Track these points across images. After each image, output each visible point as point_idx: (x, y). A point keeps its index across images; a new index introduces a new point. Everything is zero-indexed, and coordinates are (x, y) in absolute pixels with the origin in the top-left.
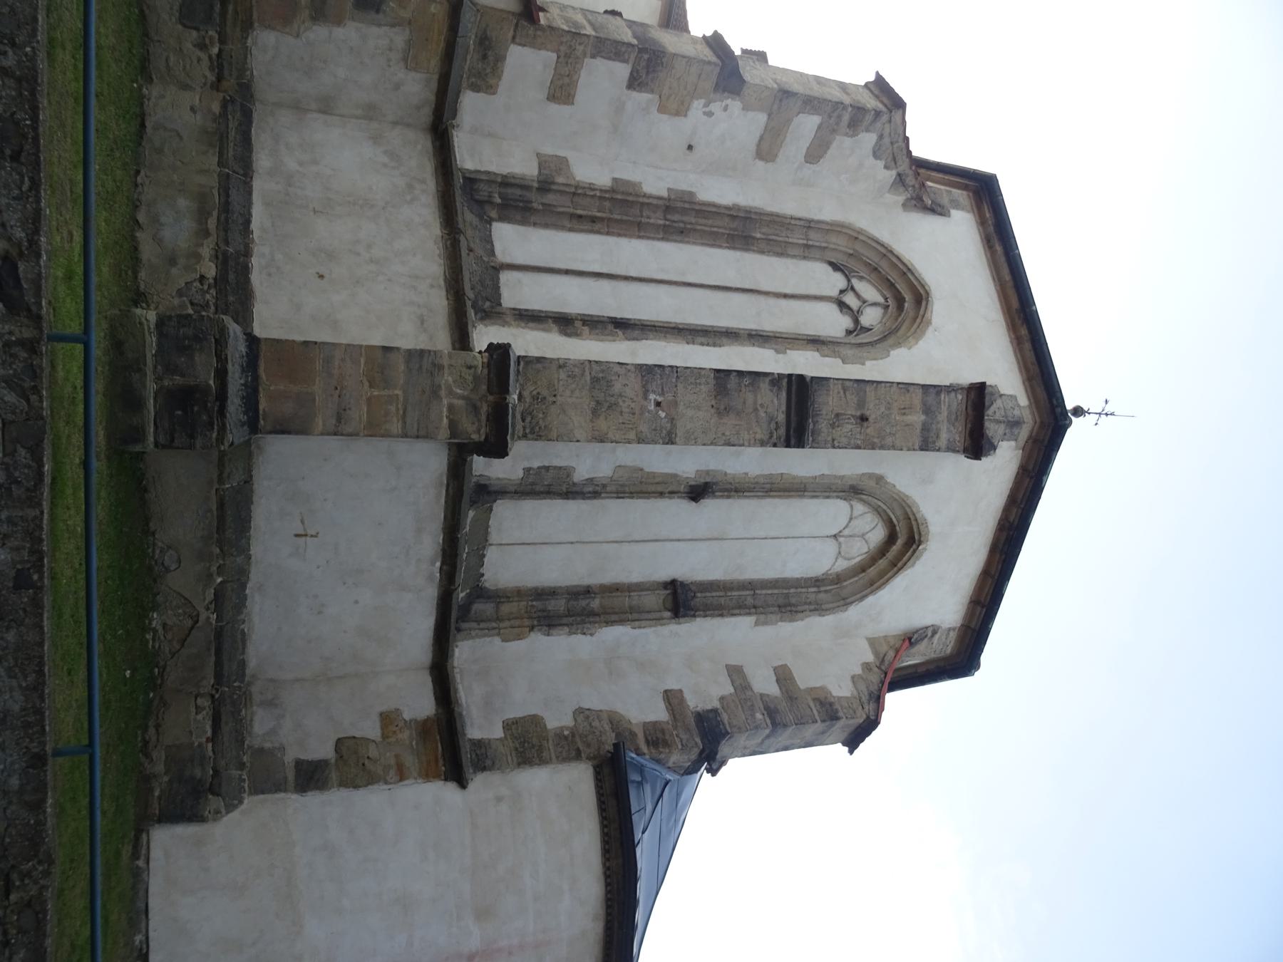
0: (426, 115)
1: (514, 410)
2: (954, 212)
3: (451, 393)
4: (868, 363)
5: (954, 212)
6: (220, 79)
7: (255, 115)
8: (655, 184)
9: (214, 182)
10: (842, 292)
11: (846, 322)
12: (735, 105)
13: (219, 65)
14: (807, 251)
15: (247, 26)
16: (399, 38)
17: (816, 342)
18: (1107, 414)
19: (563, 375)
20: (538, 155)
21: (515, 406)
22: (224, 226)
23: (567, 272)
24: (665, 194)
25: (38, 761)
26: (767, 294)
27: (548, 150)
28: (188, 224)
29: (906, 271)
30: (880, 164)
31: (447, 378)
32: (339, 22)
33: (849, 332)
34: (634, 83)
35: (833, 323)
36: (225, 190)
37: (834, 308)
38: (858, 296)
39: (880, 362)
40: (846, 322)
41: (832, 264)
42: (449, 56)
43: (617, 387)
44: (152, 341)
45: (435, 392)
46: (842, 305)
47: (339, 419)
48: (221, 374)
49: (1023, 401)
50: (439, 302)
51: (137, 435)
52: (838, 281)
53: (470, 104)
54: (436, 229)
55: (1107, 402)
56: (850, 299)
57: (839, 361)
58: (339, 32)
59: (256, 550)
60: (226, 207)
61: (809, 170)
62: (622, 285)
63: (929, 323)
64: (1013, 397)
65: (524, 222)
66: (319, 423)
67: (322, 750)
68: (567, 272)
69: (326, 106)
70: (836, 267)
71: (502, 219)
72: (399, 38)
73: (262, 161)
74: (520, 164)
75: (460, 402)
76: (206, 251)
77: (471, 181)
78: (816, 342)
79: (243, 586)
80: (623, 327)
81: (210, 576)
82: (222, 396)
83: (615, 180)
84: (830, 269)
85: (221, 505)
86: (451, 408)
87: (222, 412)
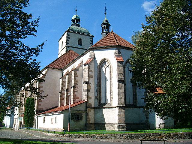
48: (121, 125)
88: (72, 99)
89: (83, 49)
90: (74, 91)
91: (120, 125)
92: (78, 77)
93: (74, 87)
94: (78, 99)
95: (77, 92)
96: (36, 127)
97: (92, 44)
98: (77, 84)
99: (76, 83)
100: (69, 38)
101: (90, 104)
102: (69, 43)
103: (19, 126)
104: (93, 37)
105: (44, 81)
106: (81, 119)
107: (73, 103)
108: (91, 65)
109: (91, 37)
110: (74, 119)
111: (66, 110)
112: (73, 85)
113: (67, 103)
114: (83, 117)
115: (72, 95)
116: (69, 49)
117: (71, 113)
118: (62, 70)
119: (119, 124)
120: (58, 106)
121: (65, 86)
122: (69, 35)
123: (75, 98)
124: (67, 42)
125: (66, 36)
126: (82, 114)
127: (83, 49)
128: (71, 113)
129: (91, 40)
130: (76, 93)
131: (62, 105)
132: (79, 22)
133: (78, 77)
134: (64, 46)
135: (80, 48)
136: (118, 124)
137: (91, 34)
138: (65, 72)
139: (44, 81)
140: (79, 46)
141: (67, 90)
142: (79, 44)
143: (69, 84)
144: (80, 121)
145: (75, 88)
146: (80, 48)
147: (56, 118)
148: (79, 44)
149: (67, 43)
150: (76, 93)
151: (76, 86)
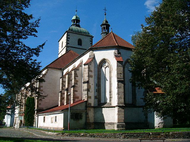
34: (89, 91)
37: (106, 69)
48: (121, 125)
58: (90, 116)
67: (145, 117)
73: (99, 121)
88: (72, 99)
90: (74, 91)
92: (77, 76)
94: (78, 98)
95: (77, 91)
96: (36, 126)
97: (92, 44)
98: (77, 84)
99: (75, 82)
100: (69, 38)
102: (69, 43)
104: (93, 37)
106: (81, 118)
107: (72, 103)
109: (91, 38)
110: (74, 117)
114: (82, 116)
115: (72, 94)
117: (71, 112)
119: (119, 124)
121: (65, 86)
122: (69, 35)
124: (67, 42)
128: (71, 113)
129: (91, 40)
130: (76, 93)
132: (79, 22)
133: (77, 76)
135: (80, 48)
137: (91, 34)
138: (65, 72)
140: (79, 47)
142: (79, 44)
143: (69, 83)
144: (80, 120)
146: (80, 48)
147: (56, 117)
148: (79, 44)
149: (67, 43)
150: (76, 93)
151: (76, 85)
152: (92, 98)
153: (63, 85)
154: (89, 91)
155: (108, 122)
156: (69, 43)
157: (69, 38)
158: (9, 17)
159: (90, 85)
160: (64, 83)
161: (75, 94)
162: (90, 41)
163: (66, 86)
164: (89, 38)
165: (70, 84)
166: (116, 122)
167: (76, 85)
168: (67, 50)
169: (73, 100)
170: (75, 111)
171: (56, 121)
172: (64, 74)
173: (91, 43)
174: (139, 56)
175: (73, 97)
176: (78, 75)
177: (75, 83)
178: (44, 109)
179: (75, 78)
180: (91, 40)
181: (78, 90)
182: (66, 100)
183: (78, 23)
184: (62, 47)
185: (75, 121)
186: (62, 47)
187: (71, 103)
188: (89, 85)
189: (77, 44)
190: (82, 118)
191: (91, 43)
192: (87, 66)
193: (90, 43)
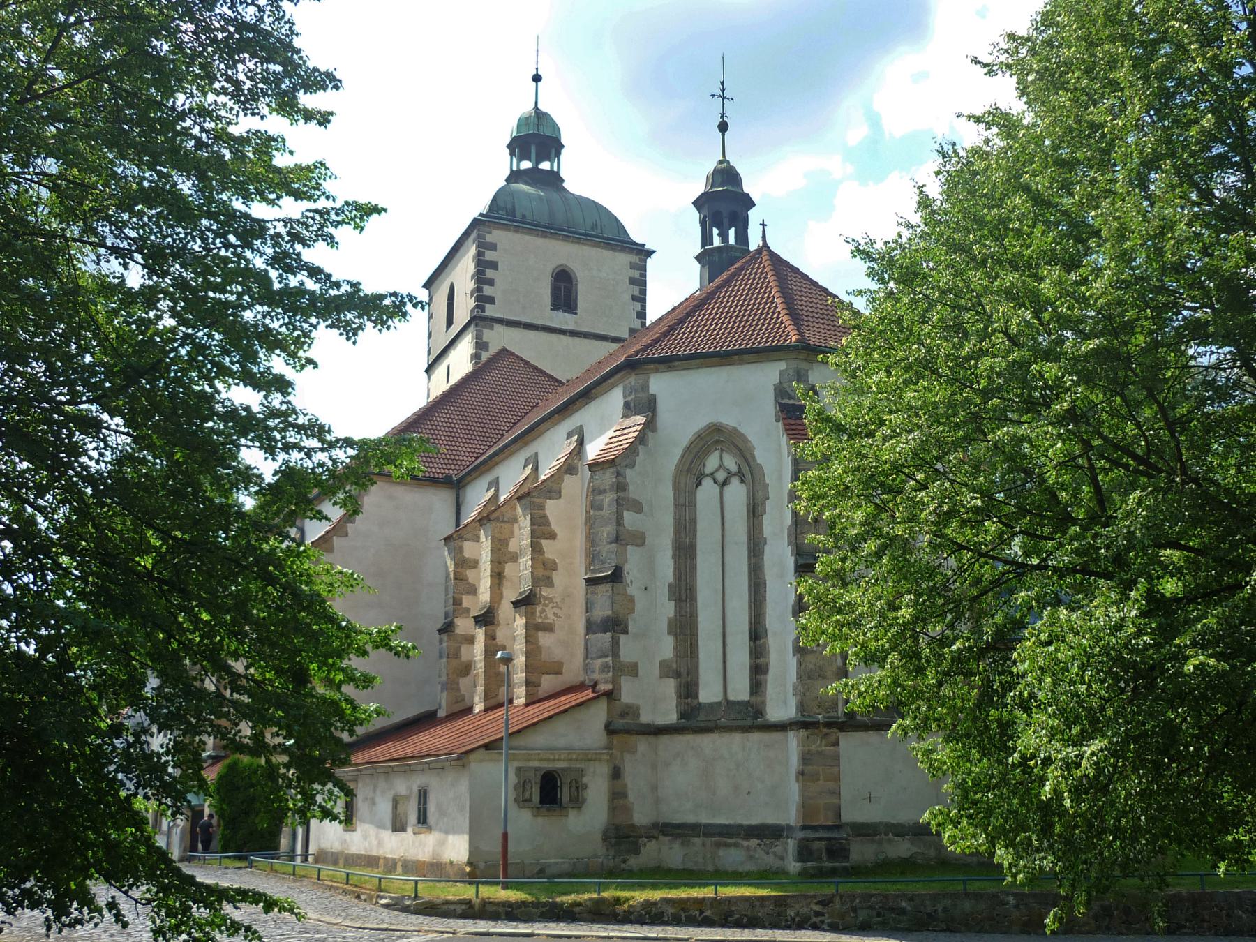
0: (651, 739)
1: (828, 718)
2: (652, 391)
3: (820, 746)
4: (767, 481)
5: (652, 391)
6: (654, 837)
7: (667, 821)
8: (668, 609)
9: (709, 841)
10: (715, 482)
11: (735, 481)
12: (626, 568)
13: (650, 837)
14: (692, 504)
15: (633, 827)
16: (627, 757)
17: (755, 511)
18: (723, 91)
19: (808, 694)
20: (661, 677)
21: (824, 717)
22: (731, 836)
23: (724, 662)
24: (673, 603)
25: (967, 895)
26: (723, 536)
27: (657, 672)
28: (732, 851)
29: (699, 436)
30: (638, 460)
31: (814, 748)
32: (625, 785)
33: (742, 481)
34: (625, 632)
35: (737, 493)
36: (711, 835)
37: (727, 489)
38: (717, 470)
39: (765, 472)
40: (735, 481)
41: (697, 487)
42: (628, 732)
43: (811, 666)
44: (809, 864)
45: (820, 753)
46: (725, 483)
47: (834, 793)
48: (820, 839)
49: (783, 365)
50: (756, 736)
51: (845, 868)
52: (707, 482)
53: (645, 718)
54: (715, 736)
55: (713, 96)
56: (721, 476)
57: (767, 502)
58: (629, 785)
59: (877, 820)
60: (721, 835)
61: (645, 508)
62: (728, 630)
63: (735, 429)
64: (781, 372)
65: (697, 684)
66: (835, 801)
68: (724, 662)
69: (654, 788)
70: (699, 484)
71: (697, 697)
72: (627, 757)
74: (669, 687)
75: (823, 743)
76: (745, 843)
77: (683, 715)
78: (755, 511)
79: (893, 824)
80: (757, 634)
81: (889, 839)
82: (829, 839)
83: (669, 633)
84: (700, 487)
85: (859, 835)
86: (826, 746)
87: (834, 839)
88: (519, 676)
89: (587, 335)
90: (533, 629)
91: (815, 839)
92: (552, 536)
93: (525, 603)
94: (558, 672)
95: (549, 628)
96: (299, 850)
97: (642, 315)
98: (549, 582)
99: (540, 572)
100: (494, 265)
101: (628, 706)
102: (491, 300)
103: (182, 839)
104: (650, 253)
105: (512, 602)
106: (578, 802)
107: (523, 701)
108: (632, 465)
109: (636, 259)
110: (536, 798)
111: (487, 746)
112: (526, 587)
113: (487, 696)
114: (585, 787)
115: (519, 647)
116: (498, 338)
117: (516, 764)
118: (456, 485)
119: (809, 834)
120: (469, 710)
121: (473, 591)
122: (493, 247)
123: (535, 668)
124: (479, 289)
125: (473, 250)
126: (582, 772)
127: (587, 335)
128: (519, 770)
129: (637, 274)
130: (544, 639)
131: (492, 702)
132: (558, 154)
133: (552, 536)
134: (462, 317)
135: (562, 332)
136: (801, 835)
137: (637, 234)
138: (477, 497)
139: (512, 602)
140: (562, 319)
141: (486, 619)
142: (556, 306)
143: (498, 576)
144: (572, 814)
145: (539, 608)
146: (562, 332)
147: (423, 795)
148: (556, 306)
149: (482, 300)
150: (544, 639)
151: (545, 592)
152: (640, 673)
153: (461, 584)
154: (625, 632)
155: (746, 822)
156: (491, 300)
157: (494, 265)
158: (27, 28)
159: (630, 591)
160: (468, 572)
161: (539, 649)
162: (633, 281)
163: (484, 596)
164: (624, 259)
165: (506, 584)
166: (792, 823)
167: (545, 592)
168: (480, 346)
169: (528, 683)
170: (541, 760)
171: (423, 819)
172: (470, 515)
173: (637, 293)
174: (1167, 164)
175: (529, 668)
176: (555, 526)
177: (535, 580)
178: (483, 751)
179: (536, 548)
180: (637, 274)
181: (558, 623)
182: (481, 681)
183: (548, 158)
184: (450, 322)
185: (540, 820)
186: (450, 322)
187: (516, 702)
188: (625, 594)
189: (547, 299)
190: (584, 801)
191: (637, 293)
192: (608, 478)
193: (627, 297)
